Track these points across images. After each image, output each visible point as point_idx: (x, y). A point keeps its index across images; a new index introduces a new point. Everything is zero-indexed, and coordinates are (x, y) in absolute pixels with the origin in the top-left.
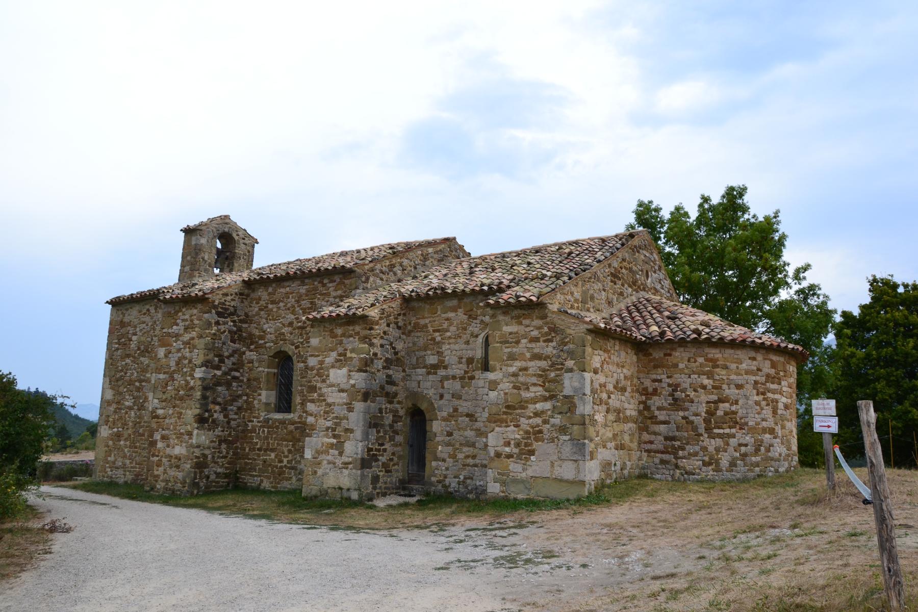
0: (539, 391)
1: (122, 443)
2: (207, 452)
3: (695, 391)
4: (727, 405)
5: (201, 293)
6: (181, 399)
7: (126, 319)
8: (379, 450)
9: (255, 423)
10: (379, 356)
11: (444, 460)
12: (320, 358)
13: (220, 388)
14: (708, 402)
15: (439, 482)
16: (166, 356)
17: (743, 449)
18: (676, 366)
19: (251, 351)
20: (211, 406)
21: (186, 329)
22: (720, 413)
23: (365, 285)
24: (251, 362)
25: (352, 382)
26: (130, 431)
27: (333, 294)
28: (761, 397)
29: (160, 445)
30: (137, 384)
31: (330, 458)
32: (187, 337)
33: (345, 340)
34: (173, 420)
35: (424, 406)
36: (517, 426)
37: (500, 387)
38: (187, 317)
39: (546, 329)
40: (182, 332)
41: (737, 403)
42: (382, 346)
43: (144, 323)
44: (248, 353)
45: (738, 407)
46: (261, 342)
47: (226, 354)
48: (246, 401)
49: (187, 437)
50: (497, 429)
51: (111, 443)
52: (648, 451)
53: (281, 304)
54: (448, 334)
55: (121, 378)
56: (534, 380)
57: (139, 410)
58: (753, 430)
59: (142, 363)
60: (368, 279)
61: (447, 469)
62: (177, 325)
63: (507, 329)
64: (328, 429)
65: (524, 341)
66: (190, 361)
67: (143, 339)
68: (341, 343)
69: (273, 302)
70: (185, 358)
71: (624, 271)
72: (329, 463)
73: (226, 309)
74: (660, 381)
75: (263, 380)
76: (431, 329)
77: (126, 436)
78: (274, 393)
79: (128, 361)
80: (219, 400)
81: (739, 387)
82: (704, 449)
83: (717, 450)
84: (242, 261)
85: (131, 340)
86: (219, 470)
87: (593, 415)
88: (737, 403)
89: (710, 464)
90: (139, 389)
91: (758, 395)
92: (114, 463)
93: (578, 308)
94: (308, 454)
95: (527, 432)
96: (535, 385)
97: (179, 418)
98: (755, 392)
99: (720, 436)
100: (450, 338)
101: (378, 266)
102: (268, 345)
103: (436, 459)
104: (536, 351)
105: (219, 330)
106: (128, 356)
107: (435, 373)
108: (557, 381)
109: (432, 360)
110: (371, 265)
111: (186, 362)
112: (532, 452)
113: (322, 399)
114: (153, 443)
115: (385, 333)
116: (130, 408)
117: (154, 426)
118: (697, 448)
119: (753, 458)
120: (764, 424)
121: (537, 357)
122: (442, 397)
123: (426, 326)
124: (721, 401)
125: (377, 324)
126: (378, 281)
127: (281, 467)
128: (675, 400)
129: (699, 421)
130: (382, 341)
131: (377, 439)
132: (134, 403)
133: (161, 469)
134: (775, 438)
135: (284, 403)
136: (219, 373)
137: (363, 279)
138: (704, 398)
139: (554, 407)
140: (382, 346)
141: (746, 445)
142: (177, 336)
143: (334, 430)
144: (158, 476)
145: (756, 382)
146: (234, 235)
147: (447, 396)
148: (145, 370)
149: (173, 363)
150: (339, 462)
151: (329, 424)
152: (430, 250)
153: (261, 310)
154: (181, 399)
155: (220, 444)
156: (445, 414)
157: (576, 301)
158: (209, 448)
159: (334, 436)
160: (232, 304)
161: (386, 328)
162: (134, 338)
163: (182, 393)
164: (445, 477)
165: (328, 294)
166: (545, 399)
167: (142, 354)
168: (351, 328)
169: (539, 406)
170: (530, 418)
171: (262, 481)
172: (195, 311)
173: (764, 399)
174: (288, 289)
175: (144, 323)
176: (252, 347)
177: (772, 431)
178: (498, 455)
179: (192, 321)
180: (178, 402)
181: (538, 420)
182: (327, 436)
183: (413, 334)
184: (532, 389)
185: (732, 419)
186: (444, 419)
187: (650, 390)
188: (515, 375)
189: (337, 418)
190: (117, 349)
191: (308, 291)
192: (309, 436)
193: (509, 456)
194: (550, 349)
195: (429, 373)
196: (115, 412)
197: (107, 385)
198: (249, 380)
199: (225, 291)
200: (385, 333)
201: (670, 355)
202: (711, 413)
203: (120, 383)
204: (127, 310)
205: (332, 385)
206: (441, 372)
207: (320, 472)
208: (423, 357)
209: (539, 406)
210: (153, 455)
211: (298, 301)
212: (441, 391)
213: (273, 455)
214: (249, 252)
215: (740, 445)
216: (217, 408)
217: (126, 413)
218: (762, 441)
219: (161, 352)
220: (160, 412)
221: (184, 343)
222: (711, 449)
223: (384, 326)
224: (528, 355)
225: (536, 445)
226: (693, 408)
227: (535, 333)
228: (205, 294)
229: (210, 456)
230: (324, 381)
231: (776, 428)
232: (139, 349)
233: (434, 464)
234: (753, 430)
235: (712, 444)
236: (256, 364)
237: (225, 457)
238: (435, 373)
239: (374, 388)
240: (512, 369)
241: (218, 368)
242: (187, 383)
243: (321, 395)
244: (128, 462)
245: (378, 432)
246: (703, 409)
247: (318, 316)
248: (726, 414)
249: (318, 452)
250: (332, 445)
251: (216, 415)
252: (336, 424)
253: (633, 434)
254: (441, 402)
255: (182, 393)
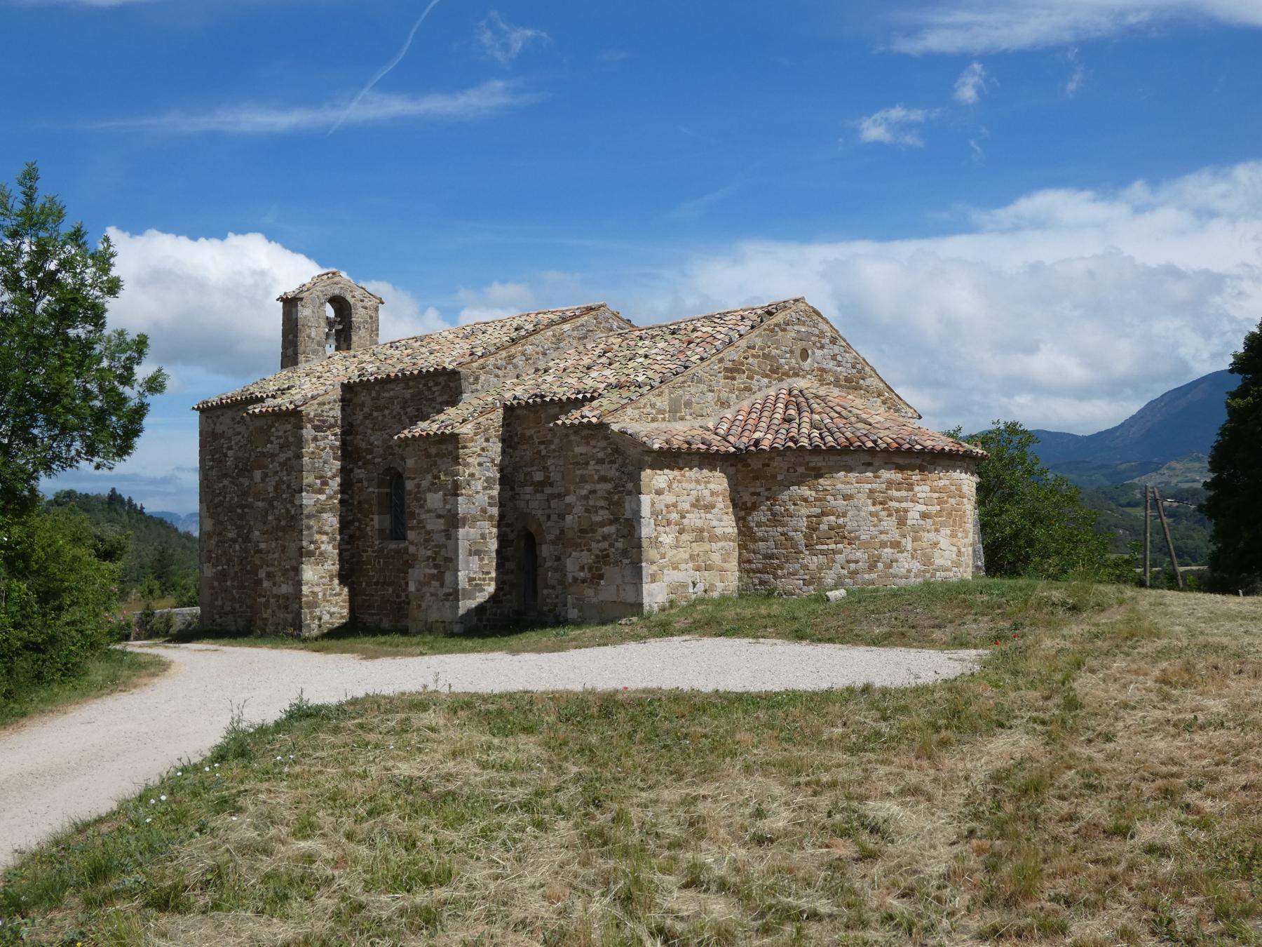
0: (603, 515)
1: (229, 583)
2: (316, 589)
3: (795, 504)
4: (832, 518)
5: (292, 407)
6: (283, 529)
7: (219, 429)
8: (484, 579)
9: (370, 553)
10: (477, 476)
11: (553, 587)
12: (416, 481)
13: (325, 515)
14: (808, 517)
15: (550, 611)
16: (263, 480)
17: (853, 566)
18: (775, 477)
19: (359, 468)
20: (317, 537)
21: (281, 447)
22: (824, 527)
23: (474, 387)
24: (360, 481)
25: (448, 507)
26: (237, 568)
27: (439, 399)
28: (879, 507)
29: (266, 584)
30: (239, 511)
31: (432, 590)
32: (282, 457)
33: (439, 461)
34: (276, 555)
35: (533, 529)
36: (589, 550)
37: (575, 511)
38: (281, 433)
39: (609, 450)
40: (277, 451)
41: (844, 515)
42: (480, 464)
43: (239, 433)
44: (357, 471)
45: (847, 520)
46: (369, 457)
47: (329, 474)
48: (359, 528)
49: (292, 574)
50: (574, 554)
51: (216, 584)
52: (748, 572)
53: (387, 412)
54: (553, 447)
55: (220, 504)
56: (602, 503)
57: (244, 542)
58: (866, 545)
59: (242, 484)
60: (477, 379)
61: (557, 597)
62: (272, 443)
63: (579, 450)
64: (429, 558)
65: (592, 463)
66: (289, 486)
67: (240, 454)
68: (435, 464)
69: (377, 409)
70: (283, 482)
71: (751, 360)
72: (432, 595)
73: (324, 422)
74: (758, 494)
75: (375, 502)
76: (536, 441)
77: (232, 574)
78: (388, 516)
79: (226, 482)
80: (326, 528)
81: (847, 497)
82: (805, 567)
83: (820, 568)
84: (362, 332)
85: (226, 455)
86: (333, 610)
87: (657, 538)
88: (844, 515)
89: (811, 583)
90: (241, 517)
91: (874, 504)
92: (222, 607)
93: (664, 419)
94: (412, 587)
95: (597, 556)
96: (602, 508)
97: (283, 551)
98: (870, 501)
99: (822, 552)
100: (554, 451)
101: (491, 360)
102: (376, 460)
103: (547, 587)
104: (602, 473)
105: (317, 447)
106: (225, 476)
107: (542, 492)
108: (619, 504)
109: (538, 476)
110: (482, 360)
111: (284, 487)
112: (601, 577)
113: (421, 525)
114: (260, 582)
115: (483, 449)
116: (234, 541)
117: (258, 562)
118: (797, 566)
119: (866, 576)
120: (883, 537)
121: (603, 479)
122: (549, 517)
123: (531, 437)
124: (823, 514)
125: (472, 440)
126: (493, 379)
127: (400, 603)
128: (774, 515)
129: (799, 537)
130: (481, 460)
131: (481, 567)
132: (238, 534)
133: (269, 611)
134: (902, 552)
135: (398, 533)
136: (322, 497)
137: (471, 380)
138: (804, 511)
139: (618, 530)
140: (480, 464)
141: (857, 562)
142: (273, 456)
143: (434, 559)
144: (267, 619)
145: (871, 491)
146: (349, 298)
147: (554, 517)
148: (245, 494)
149: (271, 489)
150: (440, 595)
151: (429, 553)
152: (566, 327)
153: (366, 418)
154: (283, 529)
155: (331, 580)
156: (552, 537)
157: (661, 412)
158: (318, 585)
159: (436, 566)
160: (331, 413)
161: (485, 444)
162: (230, 453)
163: (283, 523)
164: (556, 605)
165: (434, 400)
166: (611, 522)
167: (241, 474)
168: (444, 447)
169: (606, 530)
170: (599, 541)
171: (381, 620)
172: (289, 427)
173: (884, 509)
174: (392, 393)
175: (239, 433)
176: (360, 463)
177: (896, 545)
178: (575, 580)
179: (287, 438)
180: (280, 534)
181: (605, 545)
182: (428, 566)
183: (520, 447)
184: (601, 512)
185: (839, 534)
186: (553, 542)
187: (749, 505)
188: (586, 498)
189: (436, 546)
190: (212, 467)
191: (413, 395)
192: (412, 567)
193: (584, 581)
194: (613, 473)
195: (536, 491)
196: (217, 546)
197: (205, 514)
198: (359, 502)
199: (320, 399)
200: (483, 449)
201: (768, 465)
202: (813, 529)
203: (219, 510)
204: (218, 417)
205: (429, 511)
206: (548, 490)
207: (424, 605)
208: (530, 473)
209: (606, 530)
210: (260, 596)
211: (403, 408)
212: (548, 511)
213: (390, 590)
214: (371, 317)
215: (848, 562)
216: (325, 538)
217: (230, 546)
218: (879, 557)
219: (258, 475)
220: (262, 546)
221: (281, 464)
222: (812, 566)
223: (480, 440)
224: (596, 477)
225: (605, 569)
226: (793, 522)
227: (601, 455)
228: (297, 406)
229: (320, 595)
230: (422, 506)
231: (904, 541)
232: (237, 466)
233: (545, 592)
234: (866, 545)
235: (814, 562)
236: (366, 484)
237: (339, 594)
238: (542, 492)
239: (473, 512)
240: (584, 492)
241: (321, 491)
242: (287, 510)
243: (420, 522)
244: (237, 605)
245: (482, 560)
246: (804, 523)
247: (410, 436)
248: (831, 528)
249: (421, 584)
250: (434, 575)
251: (323, 547)
252: (436, 553)
253: (729, 554)
254: (549, 524)
255: (283, 523)
